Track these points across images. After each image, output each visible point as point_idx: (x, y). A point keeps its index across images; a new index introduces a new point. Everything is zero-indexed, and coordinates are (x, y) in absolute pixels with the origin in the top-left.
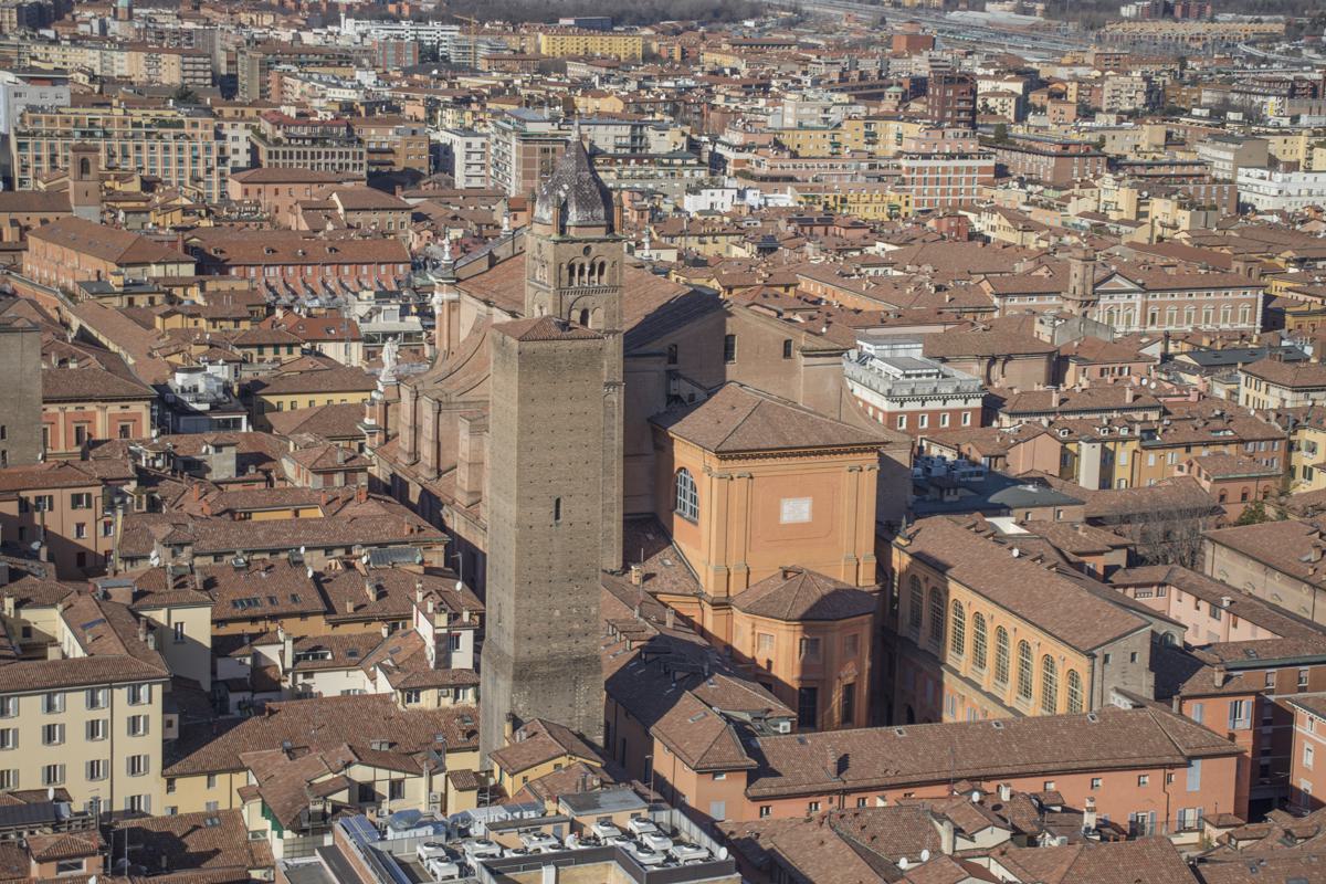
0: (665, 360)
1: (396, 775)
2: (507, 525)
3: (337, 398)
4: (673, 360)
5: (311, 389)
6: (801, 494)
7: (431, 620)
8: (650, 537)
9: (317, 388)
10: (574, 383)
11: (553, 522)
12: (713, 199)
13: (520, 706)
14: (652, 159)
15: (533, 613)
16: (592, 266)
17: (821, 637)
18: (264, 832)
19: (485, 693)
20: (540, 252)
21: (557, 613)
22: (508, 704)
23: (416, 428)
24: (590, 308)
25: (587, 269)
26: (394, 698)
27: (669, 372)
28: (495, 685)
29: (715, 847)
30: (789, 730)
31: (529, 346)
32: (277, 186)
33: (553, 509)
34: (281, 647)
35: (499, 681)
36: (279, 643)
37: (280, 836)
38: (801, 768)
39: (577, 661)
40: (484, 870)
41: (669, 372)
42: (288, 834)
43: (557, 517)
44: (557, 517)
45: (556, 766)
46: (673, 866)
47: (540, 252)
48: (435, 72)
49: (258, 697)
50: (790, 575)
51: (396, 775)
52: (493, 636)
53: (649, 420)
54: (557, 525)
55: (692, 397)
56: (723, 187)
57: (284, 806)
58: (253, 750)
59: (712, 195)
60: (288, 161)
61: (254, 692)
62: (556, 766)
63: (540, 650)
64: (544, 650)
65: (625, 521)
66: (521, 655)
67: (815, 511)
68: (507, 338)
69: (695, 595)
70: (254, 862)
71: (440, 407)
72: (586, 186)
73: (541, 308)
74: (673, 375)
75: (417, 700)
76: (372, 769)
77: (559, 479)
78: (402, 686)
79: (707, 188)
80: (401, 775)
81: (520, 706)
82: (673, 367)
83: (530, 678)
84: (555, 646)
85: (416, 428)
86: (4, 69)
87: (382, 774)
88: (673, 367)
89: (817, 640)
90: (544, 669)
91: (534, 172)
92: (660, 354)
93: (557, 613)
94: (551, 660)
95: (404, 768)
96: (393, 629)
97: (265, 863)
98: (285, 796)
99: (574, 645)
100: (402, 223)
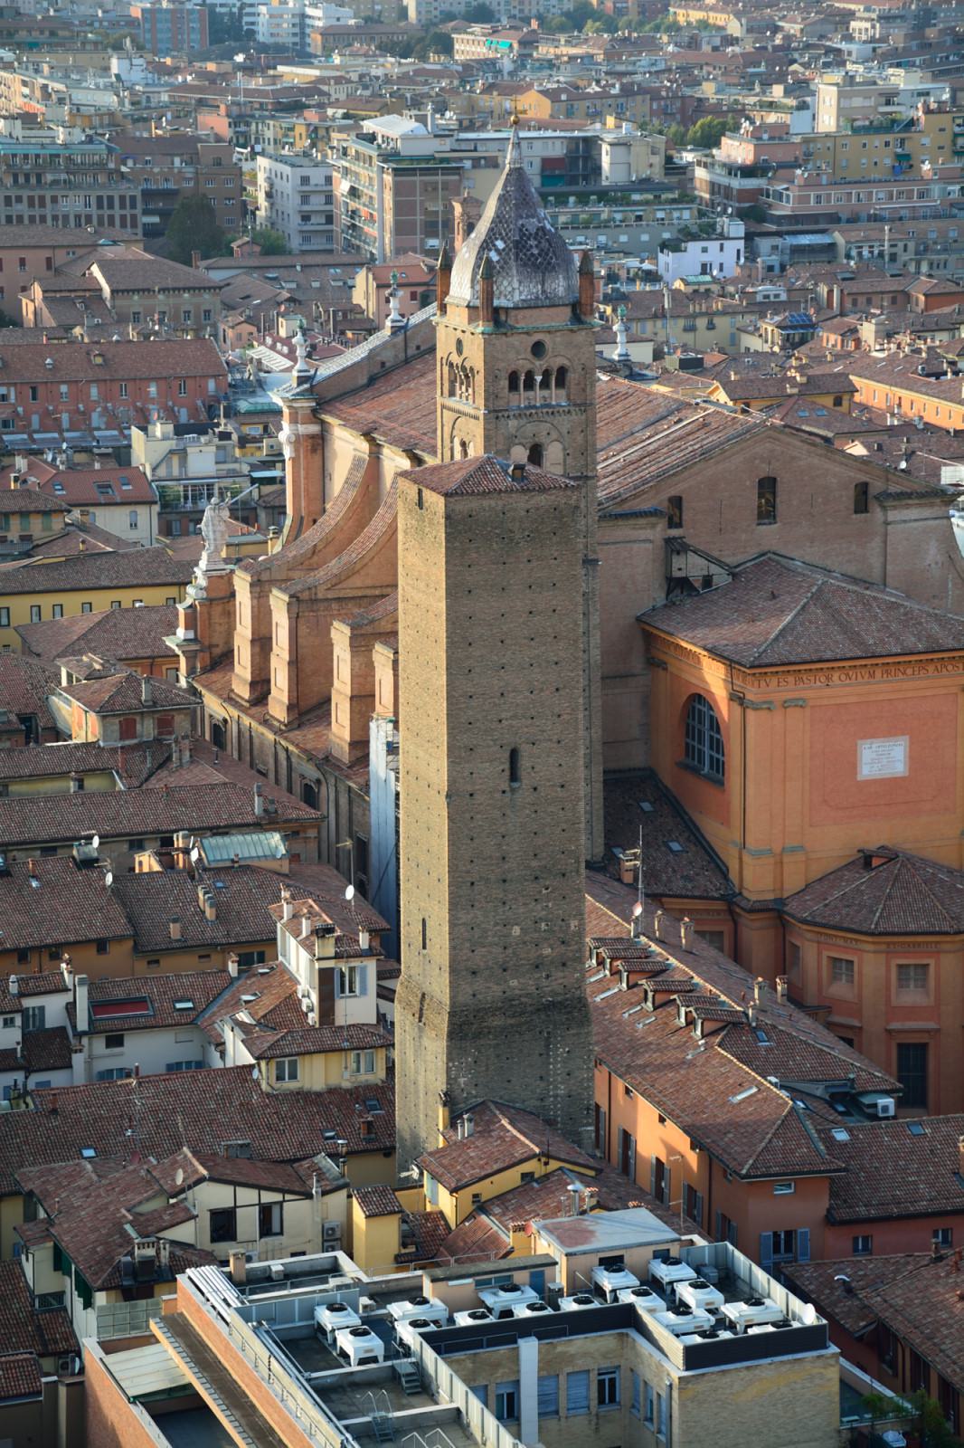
0: (662, 524)
1: (268, 1197)
2: (433, 792)
3: (126, 597)
4: (674, 523)
5: (84, 584)
6: (891, 732)
7: (308, 947)
8: (646, 806)
9: (92, 582)
10: (534, 563)
11: (505, 786)
12: (705, 258)
13: (462, 1080)
14: (604, 196)
15: (477, 932)
16: (546, 374)
17: (932, 962)
18: (59, 1296)
19: (404, 1062)
20: (460, 351)
21: (516, 931)
22: (443, 1078)
23: (262, 643)
24: (542, 439)
25: (539, 378)
26: (256, 1074)
27: (668, 541)
28: (419, 1049)
29: (796, 1304)
30: (892, 1112)
31: (464, 506)
32: (23, 254)
33: (507, 766)
34: (68, 997)
35: (426, 1042)
36: (66, 990)
37: (88, 1304)
38: (918, 1174)
39: (552, 1006)
40: (425, 1345)
41: (668, 541)
42: (101, 1298)
43: (514, 777)
44: (514, 777)
45: (524, 1176)
46: (725, 1335)
47: (460, 351)
48: (240, 58)
49: (36, 1078)
50: (875, 862)
51: (268, 1197)
52: (414, 971)
53: (638, 619)
54: (513, 790)
55: (707, 581)
56: (722, 237)
57: (94, 1251)
58: (33, 1164)
59: (705, 250)
60: (128, 212)
61: (29, 1071)
62: (524, 1176)
63: (492, 991)
64: (496, 990)
65: (605, 782)
66: (461, 999)
67: (914, 759)
68: (427, 494)
69: (722, 898)
70: (45, 1344)
71: (298, 606)
72: (532, 242)
73: (463, 444)
74: (674, 547)
75: (293, 1076)
76: (232, 1188)
77: (515, 717)
78: (269, 1054)
79: (694, 237)
80: (277, 1197)
81: (462, 1080)
82: (675, 532)
83: (478, 1035)
84: (514, 983)
85: (262, 643)
86: (3, 46)
87: (247, 1196)
88: (675, 532)
89: (926, 966)
90: (497, 1021)
91: (414, 223)
92: (655, 513)
93: (516, 931)
94: (509, 1005)
95: (281, 1184)
96: (245, 962)
97: (62, 1346)
98: (92, 1237)
99: (544, 982)
100: (207, 313)
